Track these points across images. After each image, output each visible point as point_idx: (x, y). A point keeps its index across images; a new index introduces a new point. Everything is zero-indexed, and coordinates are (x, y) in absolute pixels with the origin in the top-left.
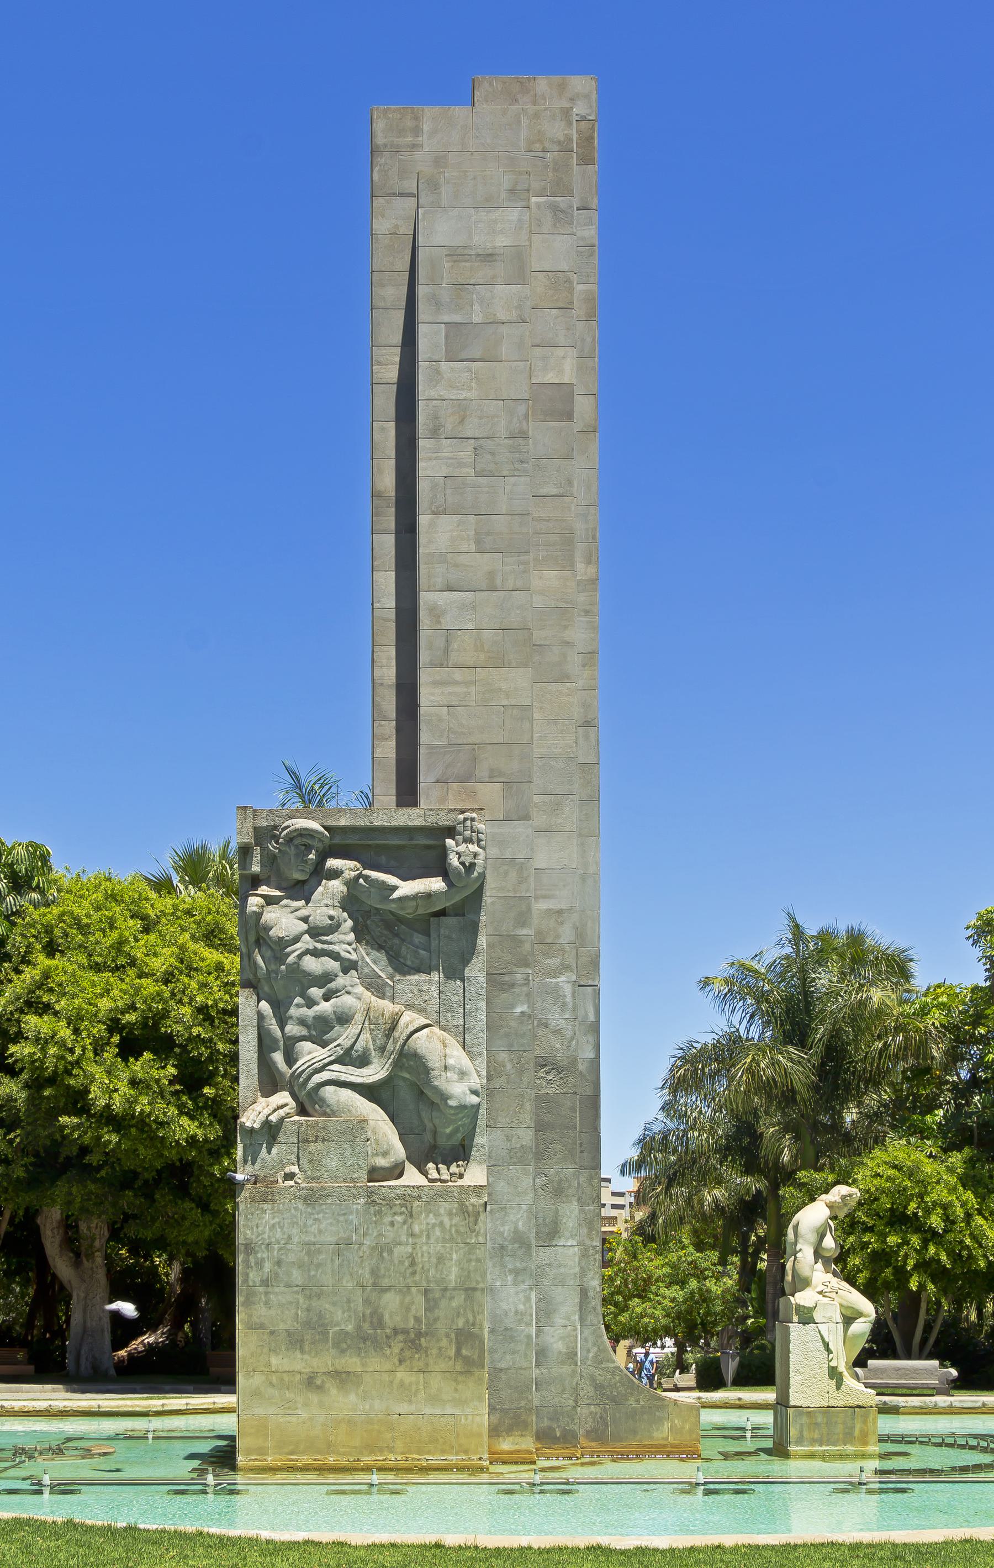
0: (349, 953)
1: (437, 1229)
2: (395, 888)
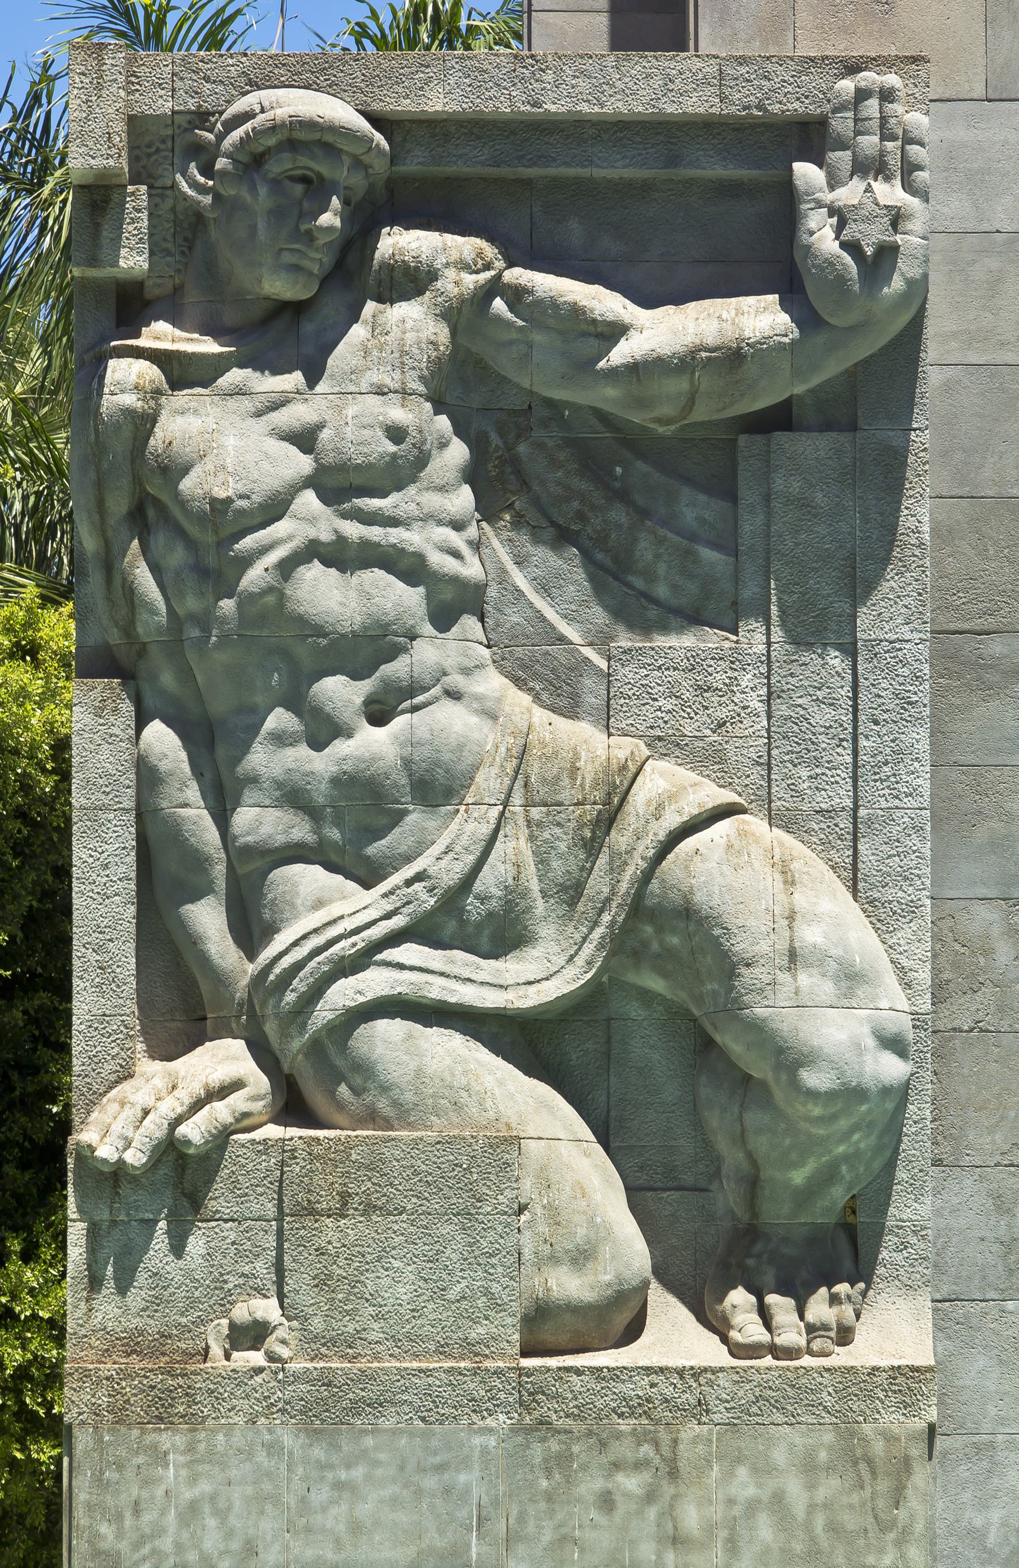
0: (457, 555)
2: (616, 331)
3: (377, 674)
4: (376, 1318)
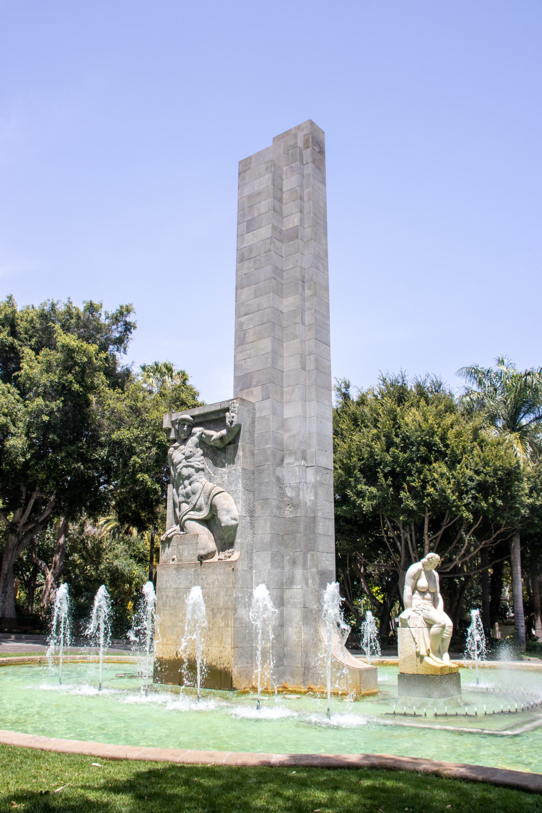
1: (216, 581)
2: (212, 436)
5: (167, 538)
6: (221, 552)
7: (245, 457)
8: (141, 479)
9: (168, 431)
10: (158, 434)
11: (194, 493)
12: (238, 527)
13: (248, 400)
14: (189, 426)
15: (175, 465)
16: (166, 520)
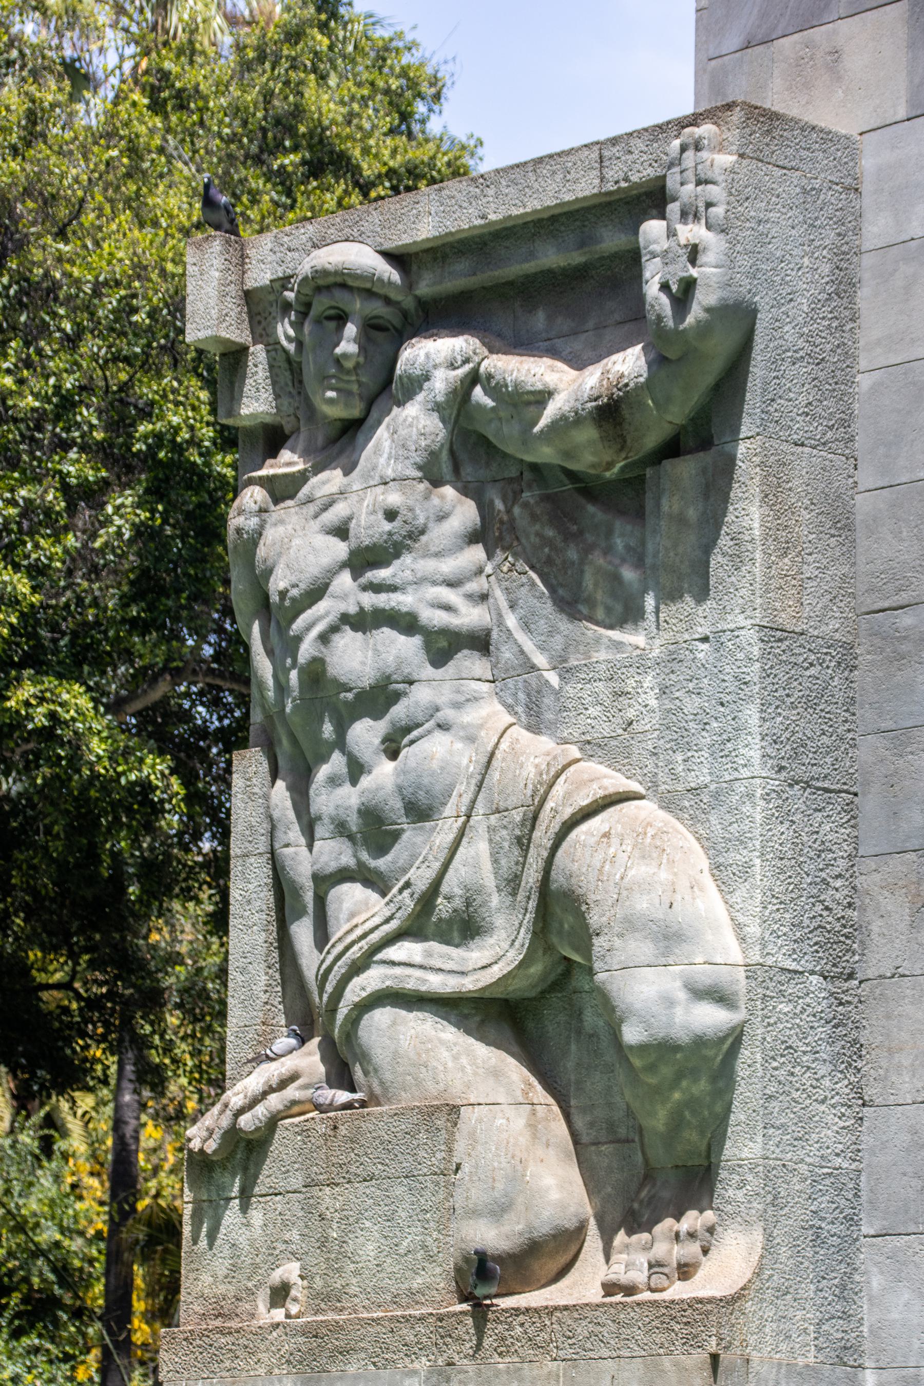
0: (448, 608)
2: (543, 397)
3: (388, 717)
4: (356, 1273)
5: (232, 1134)
6: (621, 1238)
7: (782, 542)
8: (40, 718)
9: (223, 369)
10: (147, 390)
11: (420, 811)
12: (745, 1054)
13: (810, 117)
14: (371, 328)
15: (279, 614)
16: (222, 1015)
